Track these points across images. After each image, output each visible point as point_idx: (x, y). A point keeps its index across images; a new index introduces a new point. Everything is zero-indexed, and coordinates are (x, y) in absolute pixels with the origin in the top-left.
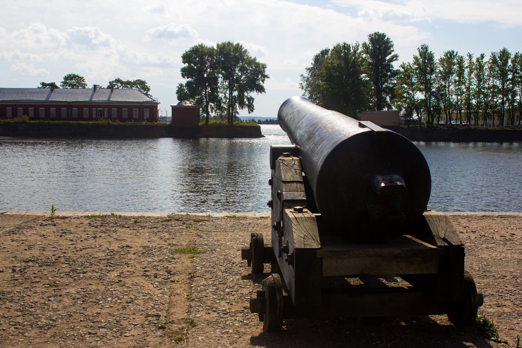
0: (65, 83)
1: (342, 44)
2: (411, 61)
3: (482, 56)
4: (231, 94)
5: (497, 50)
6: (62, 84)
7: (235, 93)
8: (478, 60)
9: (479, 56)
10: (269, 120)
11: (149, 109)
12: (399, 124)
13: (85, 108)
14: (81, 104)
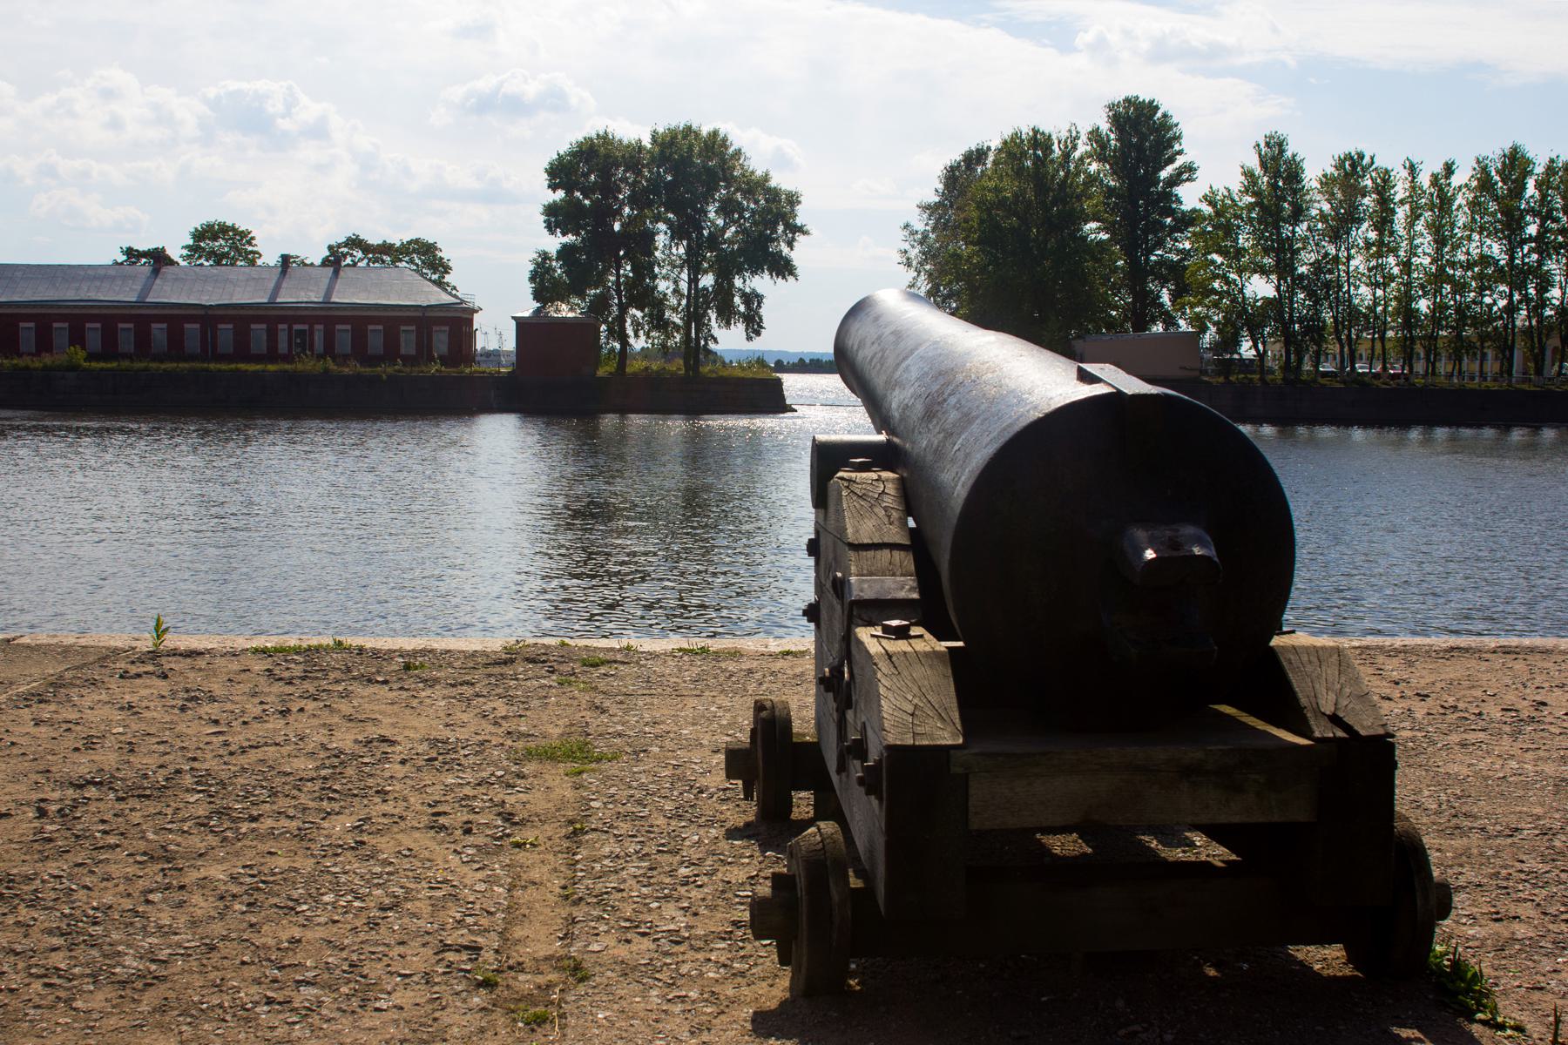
0: (195, 250)
1: (1026, 131)
2: (1234, 182)
3: (1449, 169)
4: (693, 281)
5: (1494, 151)
6: (185, 252)
7: (707, 281)
8: (1435, 180)
9: (1438, 168)
10: (808, 361)
11: (447, 328)
12: (1197, 373)
13: (255, 323)
14: (242, 312)
